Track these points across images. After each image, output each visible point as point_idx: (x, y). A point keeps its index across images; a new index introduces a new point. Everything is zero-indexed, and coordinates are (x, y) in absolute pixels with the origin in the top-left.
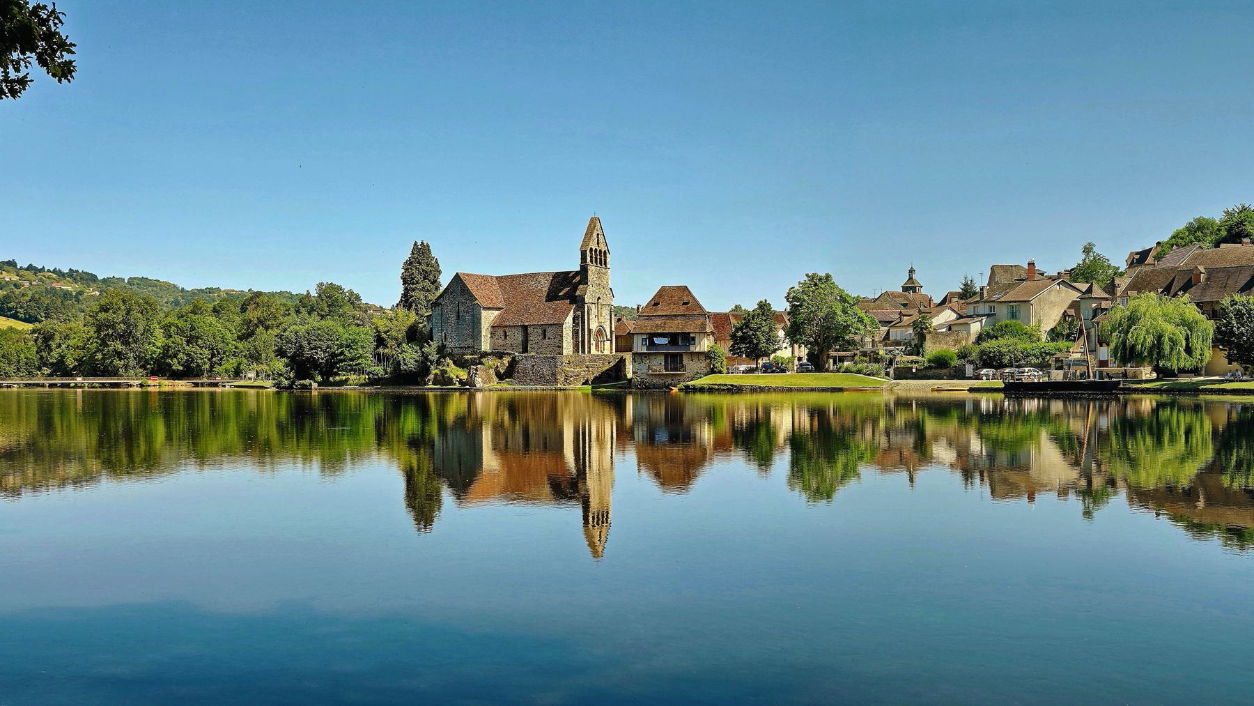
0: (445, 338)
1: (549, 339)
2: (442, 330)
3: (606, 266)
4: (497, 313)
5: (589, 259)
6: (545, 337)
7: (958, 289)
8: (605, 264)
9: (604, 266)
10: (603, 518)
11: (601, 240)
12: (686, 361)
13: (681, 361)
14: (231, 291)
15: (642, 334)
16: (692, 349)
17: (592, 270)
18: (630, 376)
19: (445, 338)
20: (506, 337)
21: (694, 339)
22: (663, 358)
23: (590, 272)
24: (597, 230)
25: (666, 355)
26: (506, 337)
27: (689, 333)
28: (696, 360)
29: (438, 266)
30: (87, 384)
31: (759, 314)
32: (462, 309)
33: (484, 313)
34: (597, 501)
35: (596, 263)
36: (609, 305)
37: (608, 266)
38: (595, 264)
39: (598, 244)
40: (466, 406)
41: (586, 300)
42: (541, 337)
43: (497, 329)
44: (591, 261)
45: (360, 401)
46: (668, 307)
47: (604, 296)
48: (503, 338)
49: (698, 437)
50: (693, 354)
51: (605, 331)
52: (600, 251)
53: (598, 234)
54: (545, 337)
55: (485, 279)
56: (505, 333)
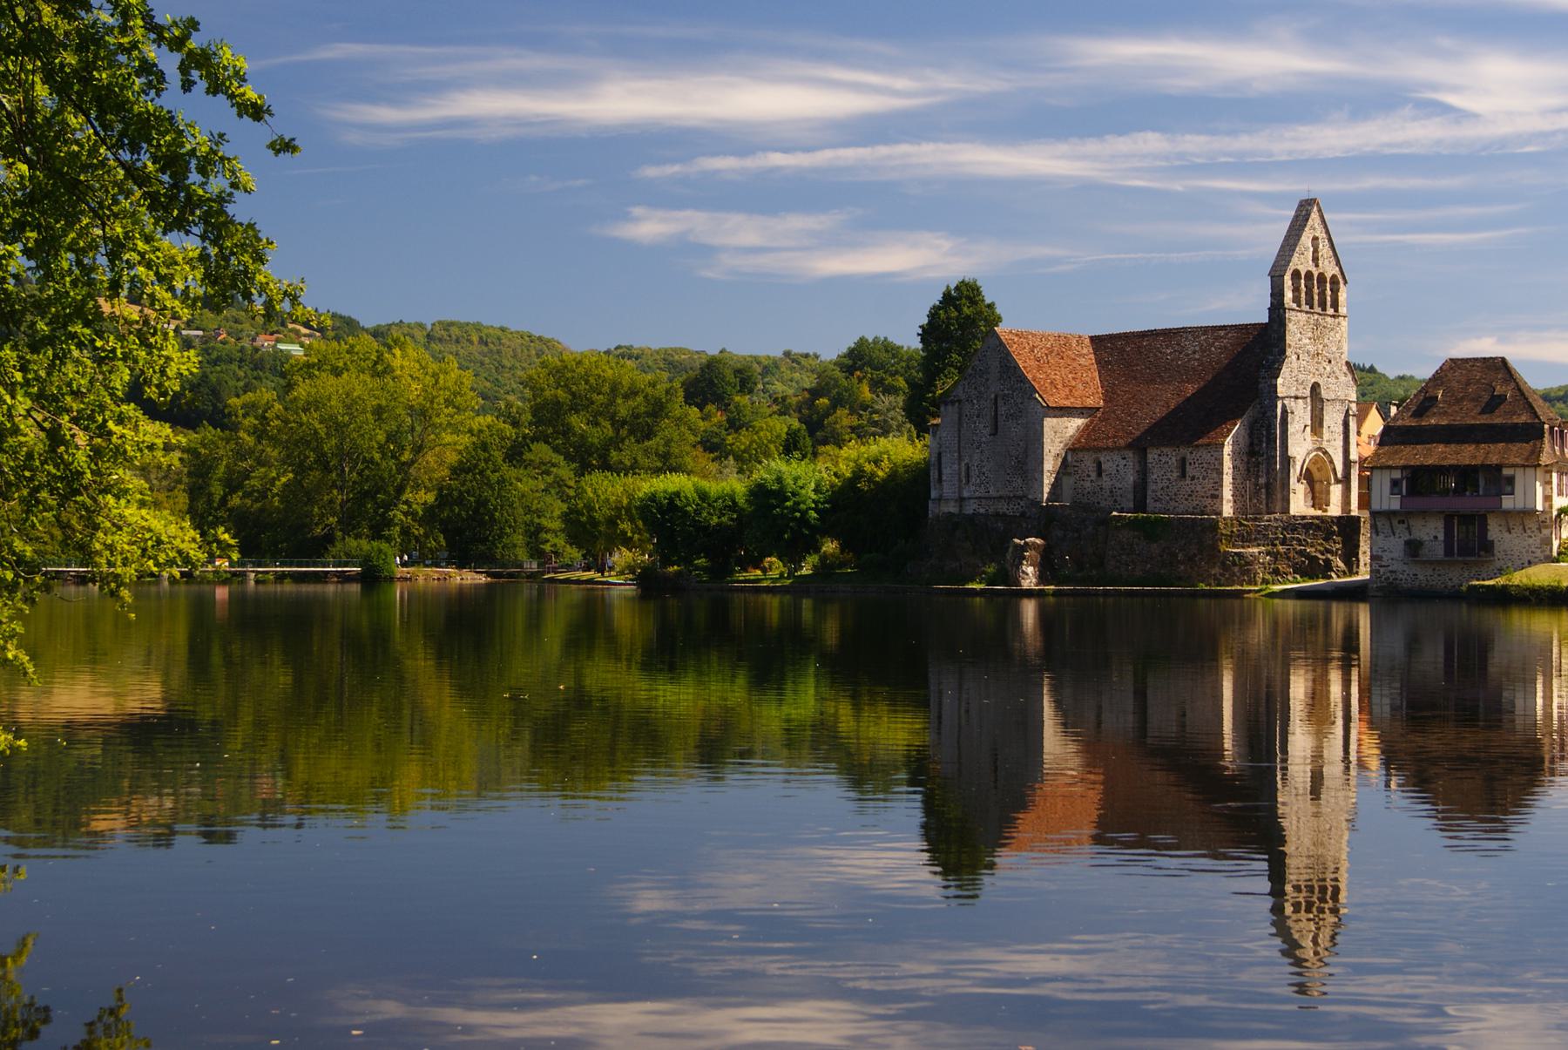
0: (968, 476)
1: (1193, 478)
2: (960, 459)
3: (1336, 310)
4: (1078, 422)
5: (1289, 295)
6: (1183, 475)
8: (1335, 305)
9: (1331, 311)
10: (1323, 895)
11: (1324, 249)
12: (1495, 531)
14: (675, 350)
15: (1390, 468)
16: (1507, 503)
19: (968, 476)
20: (1099, 474)
21: (1511, 480)
22: (1440, 525)
23: (1291, 327)
25: (1448, 519)
26: (1099, 474)
27: (1499, 468)
28: (1518, 530)
30: (378, 784)
31: (236, 444)
32: (1002, 410)
33: (1049, 423)
35: (1310, 303)
36: (1343, 401)
37: (1343, 310)
38: (1307, 308)
39: (1315, 260)
41: (1281, 391)
43: (1080, 455)
44: (1296, 300)
45: (1413, 798)
48: (1094, 475)
51: (1331, 462)
52: (1322, 277)
53: (1315, 239)
54: (1183, 475)
55: (1064, 341)
56: (1099, 465)
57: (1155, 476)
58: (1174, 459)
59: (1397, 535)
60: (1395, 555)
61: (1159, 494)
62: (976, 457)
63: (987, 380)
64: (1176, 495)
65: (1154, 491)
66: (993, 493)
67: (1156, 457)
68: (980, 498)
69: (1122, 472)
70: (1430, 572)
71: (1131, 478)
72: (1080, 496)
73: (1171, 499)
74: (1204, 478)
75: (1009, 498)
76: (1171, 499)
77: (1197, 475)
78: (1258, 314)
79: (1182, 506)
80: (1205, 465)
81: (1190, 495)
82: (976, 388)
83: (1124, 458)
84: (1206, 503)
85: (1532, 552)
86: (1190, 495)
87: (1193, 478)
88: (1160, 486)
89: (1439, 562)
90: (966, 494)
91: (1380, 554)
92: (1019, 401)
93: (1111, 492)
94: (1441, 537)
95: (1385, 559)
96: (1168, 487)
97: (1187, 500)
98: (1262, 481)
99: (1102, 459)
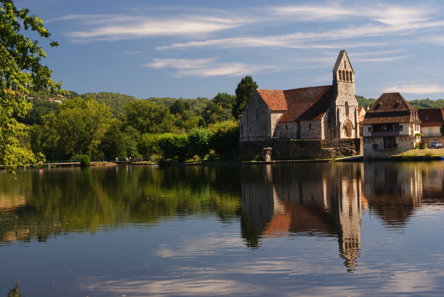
0: (250, 131)
1: (313, 129)
6: (310, 128)
7: (88, 93)
8: (351, 79)
9: (350, 81)
12: (398, 141)
13: (395, 141)
15: (368, 124)
16: (401, 133)
17: (341, 86)
18: (60, 137)
19: (250, 131)
21: (402, 127)
24: (344, 58)
25: (385, 138)
27: (398, 123)
28: (404, 140)
29: (74, 95)
32: (259, 112)
33: (272, 115)
34: (349, 229)
36: (354, 106)
38: (343, 80)
39: (345, 67)
40: (384, 178)
42: (308, 128)
43: (281, 124)
44: (340, 78)
46: (386, 107)
47: (351, 100)
48: (285, 129)
49: (406, 192)
50: (401, 136)
51: (352, 123)
52: (347, 72)
53: (345, 61)
54: (310, 128)
56: (287, 126)
57: (302, 129)
58: (308, 124)
59: (371, 143)
60: (370, 149)
61: (304, 134)
62: (252, 125)
63: (255, 104)
64: (308, 134)
65: (302, 133)
66: (257, 135)
67: (303, 123)
68: (254, 137)
69: (293, 128)
70: (380, 153)
71: (296, 130)
72: (282, 135)
73: (307, 135)
74: (316, 129)
75: (262, 136)
76: (307, 135)
77: (314, 128)
78: (331, 84)
79: (310, 137)
80: (316, 125)
81: (312, 134)
82: (251, 106)
83: (294, 124)
84: (317, 136)
85: (408, 147)
86: (312, 134)
87: (313, 129)
88: (304, 132)
89: (383, 150)
90: (250, 136)
91: (366, 148)
92: (264, 109)
93: (290, 134)
94: (383, 143)
95: (367, 150)
96: (306, 132)
97: (312, 135)
98: (332, 129)
99: (288, 125)
